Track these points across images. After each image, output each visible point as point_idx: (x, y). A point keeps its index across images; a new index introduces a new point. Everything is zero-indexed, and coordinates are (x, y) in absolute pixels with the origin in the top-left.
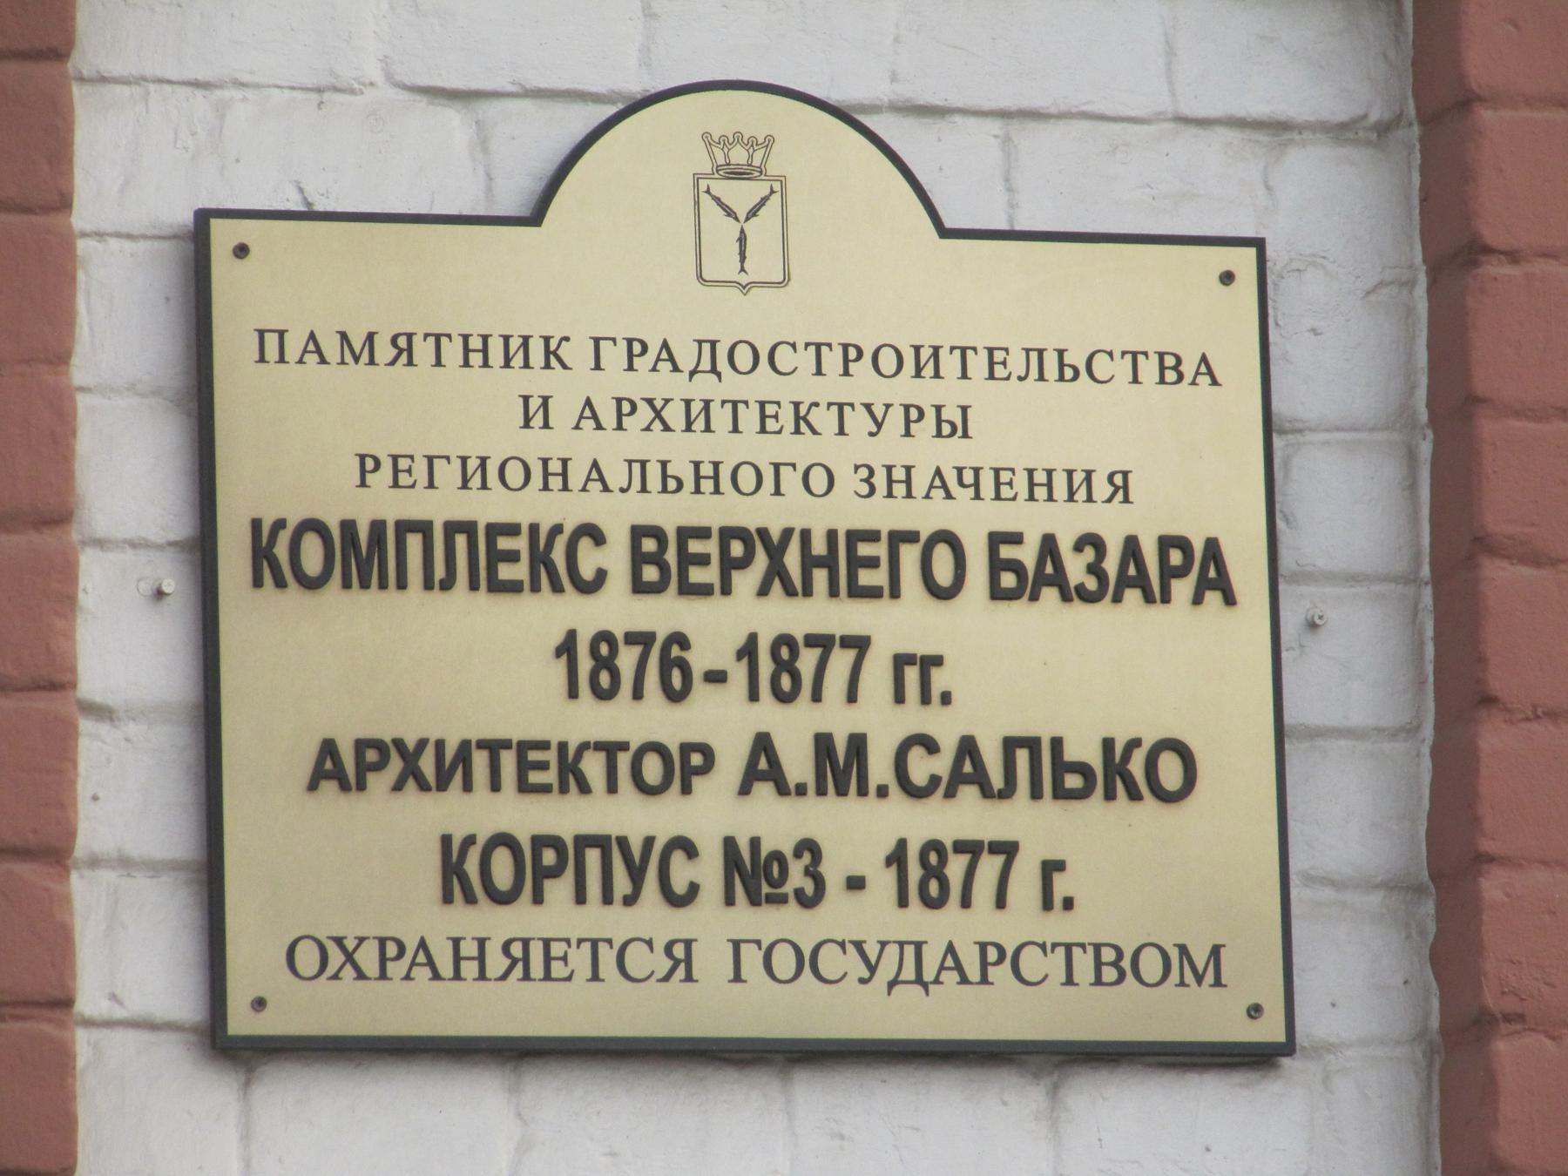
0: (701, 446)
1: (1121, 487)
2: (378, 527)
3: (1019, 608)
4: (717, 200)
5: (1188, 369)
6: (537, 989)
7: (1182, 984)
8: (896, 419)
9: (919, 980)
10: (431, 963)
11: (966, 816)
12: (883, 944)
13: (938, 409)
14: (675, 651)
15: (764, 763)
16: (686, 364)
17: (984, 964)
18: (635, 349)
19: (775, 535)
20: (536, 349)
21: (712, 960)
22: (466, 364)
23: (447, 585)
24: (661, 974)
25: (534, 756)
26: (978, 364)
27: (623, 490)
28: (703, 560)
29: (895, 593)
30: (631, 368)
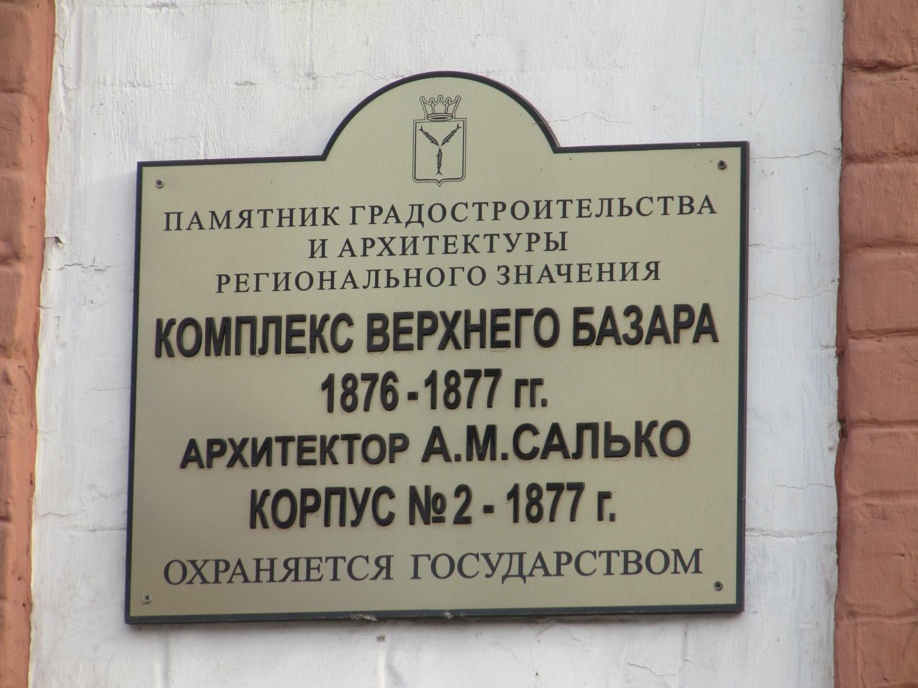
0: (411, 262)
1: (654, 270)
2: (226, 321)
3: (593, 349)
4: (427, 134)
5: (697, 205)
6: (302, 586)
7: (676, 572)
8: (523, 242)
9: (521, 574)
10: (243, 573)
11: (554, 469)
12: (501, 555)
13: (548, 234)
14: (390, 382)
15: (436, 446)
16: (404, 218)
17: (559, 564)
18: (375, 211)
19: (450, 316)
20: (320, 215)
21: (402, 567)
22: (280, 225)
24: (372, 575)
25: (307, 444)
26: (572, 209)
27: (365, 287)
28: (408, 331)
29: (518, 345)
30: (372, 222)
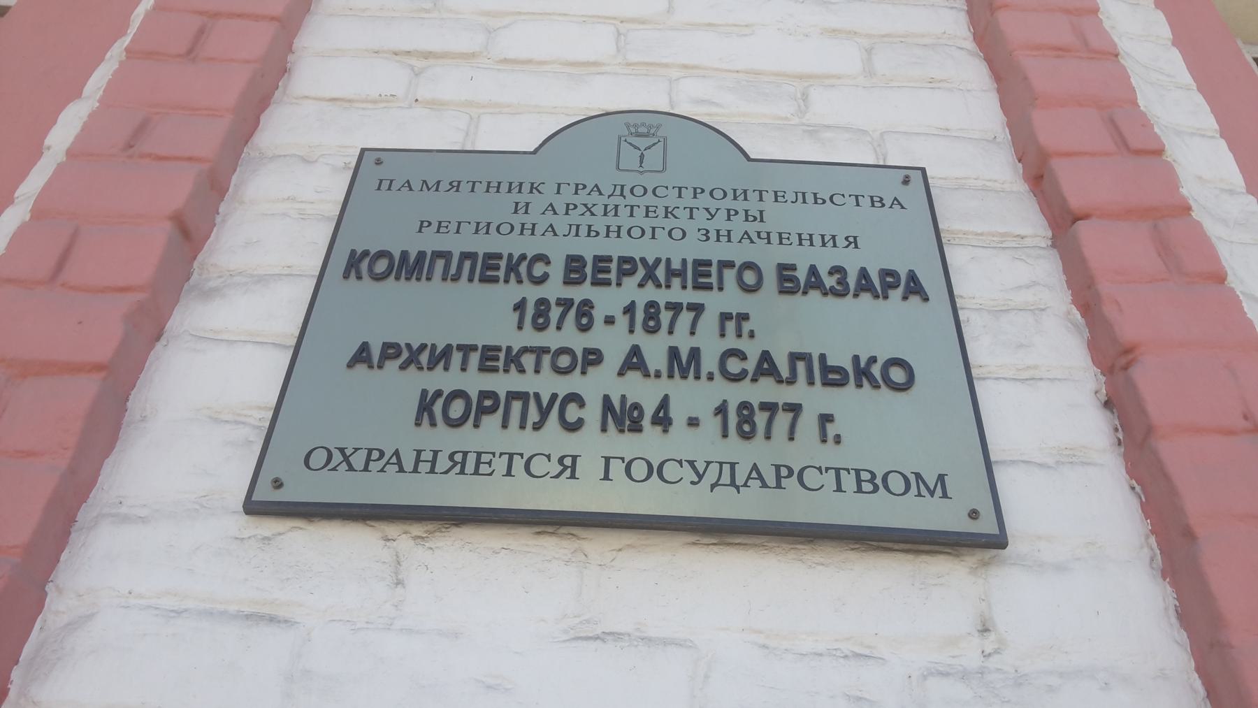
1: (853, 242)
2: (421, 255)
7: (919, 495)
9: (733, 483)
11: (766, 391)
12: (708, 463)
15: (634, 361)
17: (779, 477)
21: (590, 467)
23: (456, 278)
